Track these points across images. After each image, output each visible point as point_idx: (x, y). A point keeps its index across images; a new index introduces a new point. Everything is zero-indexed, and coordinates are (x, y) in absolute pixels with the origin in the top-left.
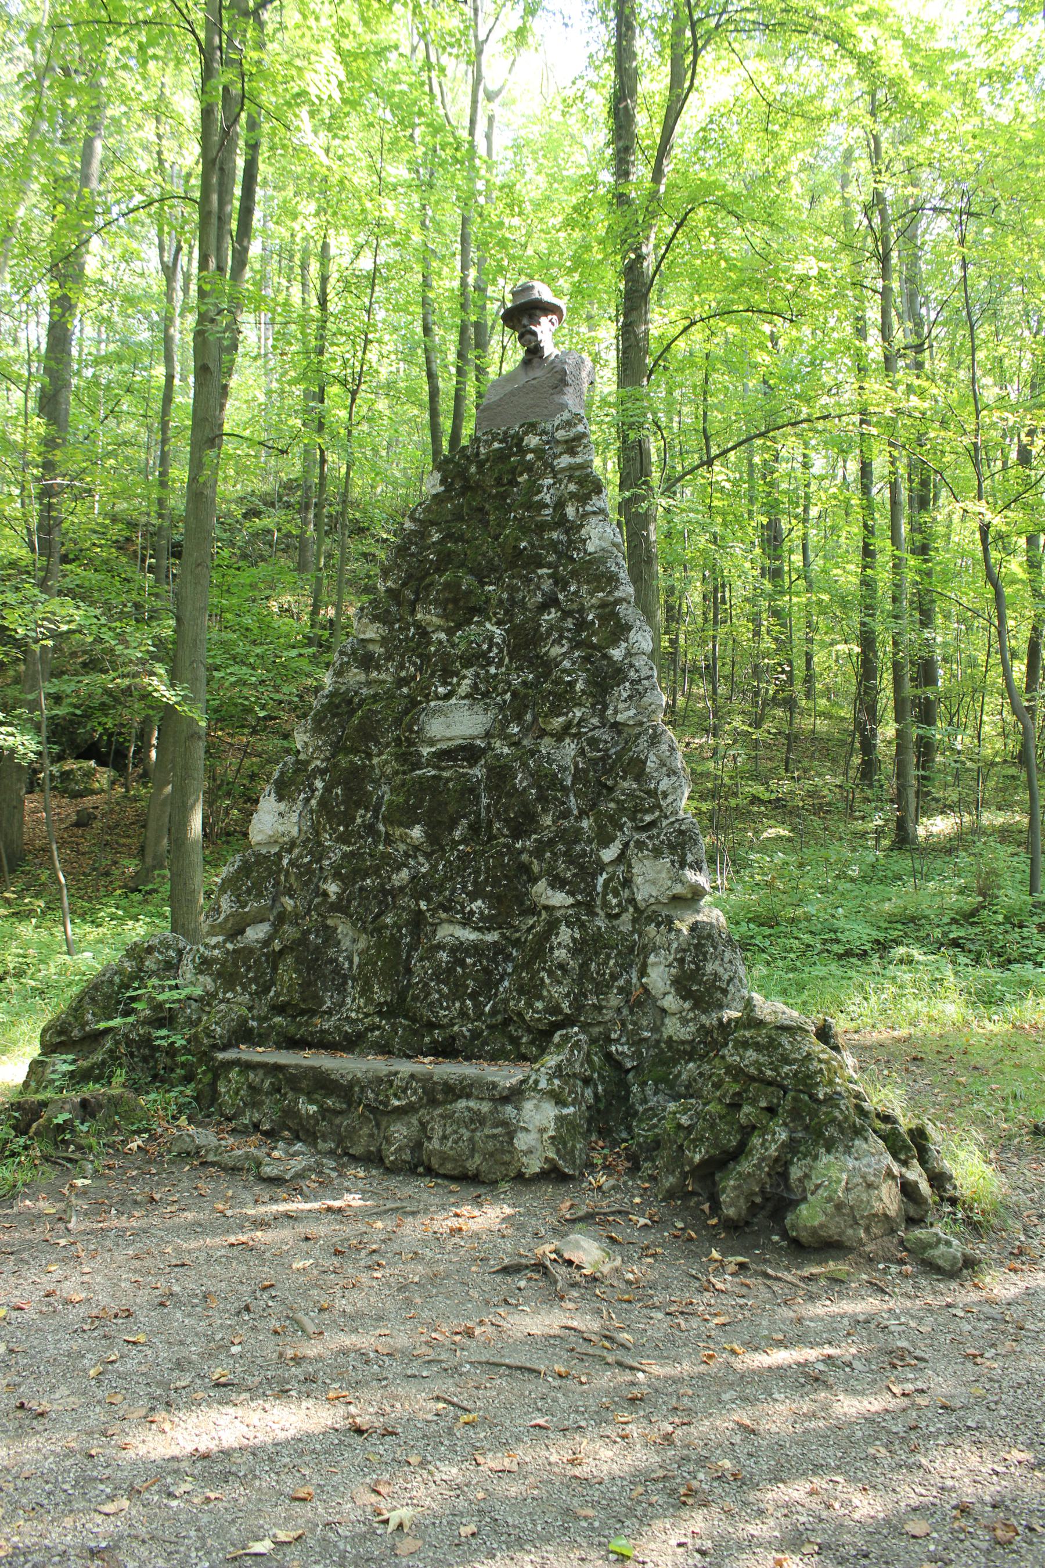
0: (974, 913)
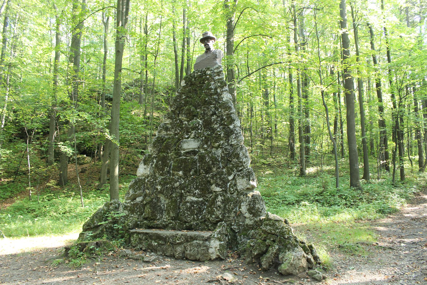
0: (322, 193)
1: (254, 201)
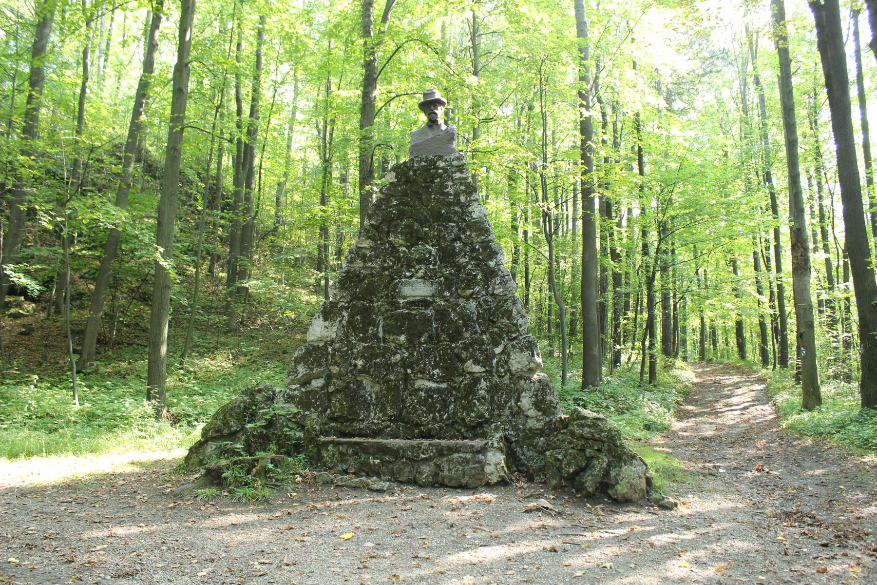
1: (543, 389)
